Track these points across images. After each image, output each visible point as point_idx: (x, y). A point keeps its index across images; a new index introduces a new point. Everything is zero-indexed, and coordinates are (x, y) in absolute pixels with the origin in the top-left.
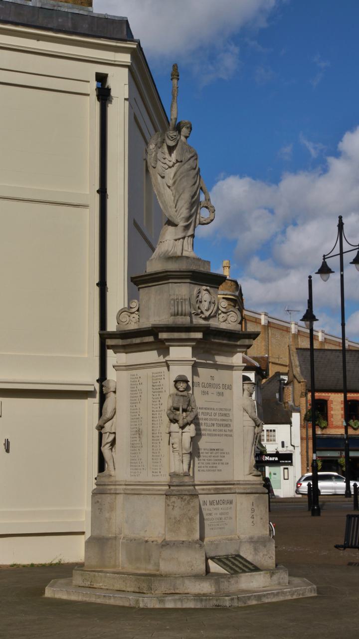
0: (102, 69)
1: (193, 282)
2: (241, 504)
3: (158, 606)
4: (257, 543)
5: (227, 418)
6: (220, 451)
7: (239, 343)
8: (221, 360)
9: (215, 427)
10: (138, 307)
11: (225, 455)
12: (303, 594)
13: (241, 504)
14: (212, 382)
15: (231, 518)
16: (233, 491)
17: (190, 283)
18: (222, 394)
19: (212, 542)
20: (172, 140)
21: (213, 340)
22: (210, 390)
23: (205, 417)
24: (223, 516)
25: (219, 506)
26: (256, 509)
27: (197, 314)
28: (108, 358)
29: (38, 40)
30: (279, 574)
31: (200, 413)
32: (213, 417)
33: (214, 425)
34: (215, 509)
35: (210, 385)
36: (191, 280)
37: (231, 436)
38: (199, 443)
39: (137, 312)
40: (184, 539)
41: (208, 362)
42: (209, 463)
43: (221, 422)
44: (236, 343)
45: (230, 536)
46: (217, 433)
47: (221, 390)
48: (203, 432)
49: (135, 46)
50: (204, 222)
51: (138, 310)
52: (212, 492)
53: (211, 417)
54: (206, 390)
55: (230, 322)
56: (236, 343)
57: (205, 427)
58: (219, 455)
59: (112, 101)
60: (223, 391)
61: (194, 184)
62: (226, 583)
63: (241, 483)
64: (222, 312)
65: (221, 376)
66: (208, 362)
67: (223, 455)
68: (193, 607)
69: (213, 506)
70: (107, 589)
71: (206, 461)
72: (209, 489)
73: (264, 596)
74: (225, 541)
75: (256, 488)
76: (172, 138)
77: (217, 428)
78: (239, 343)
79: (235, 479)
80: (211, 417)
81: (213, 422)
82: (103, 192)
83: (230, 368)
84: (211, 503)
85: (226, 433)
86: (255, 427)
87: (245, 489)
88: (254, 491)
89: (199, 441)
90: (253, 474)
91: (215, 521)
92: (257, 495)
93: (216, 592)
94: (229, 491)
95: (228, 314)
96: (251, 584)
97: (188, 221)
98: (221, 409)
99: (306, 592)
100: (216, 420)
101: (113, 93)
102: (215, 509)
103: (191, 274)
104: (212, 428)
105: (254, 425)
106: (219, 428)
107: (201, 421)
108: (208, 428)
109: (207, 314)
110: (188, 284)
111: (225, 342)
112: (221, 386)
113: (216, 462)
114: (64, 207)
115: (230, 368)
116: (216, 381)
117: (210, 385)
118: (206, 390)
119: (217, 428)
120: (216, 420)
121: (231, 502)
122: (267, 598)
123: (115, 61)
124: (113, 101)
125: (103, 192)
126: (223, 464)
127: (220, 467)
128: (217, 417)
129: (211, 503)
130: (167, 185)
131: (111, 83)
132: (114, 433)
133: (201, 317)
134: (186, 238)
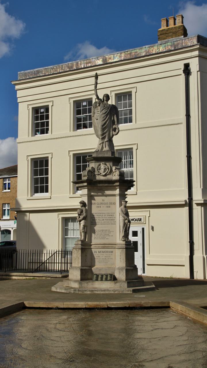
0: (186, 62)
2: (117, 253)
3: (56, 291)
4: (120, 269)
5: (113, 217)
7: (115, 185)
8: (107, 192)
12: (122, 292)
13: (117, 253)
14: (104, 202)
15: (112, 259)
16: (113, 247)
17: (95, 162)
18: (110, 207)
19: (97, 268)
21: (98, 185)
22: (102, 206)
23: (99, 217)
24: (107, 258)
26: (121, 255)
27: (98, 175)
28: (193, 189)
29: (159, 59)
30: (120, 283)
31: (96, 215)
33: (104, 220)
35: (102, 203)
36: (95, 161)
37: (115, 224)
38: (95, 228)
40: (76, 266)
41: (98, 194)
42: (98, 234)
44: (113, 185)
45: (111, 266)
47: (109, 205)
48: (97, 223)
49: (199, 47)
52: (100, 247)
56: (113, 185)
57: (99, 221)
59: (191, 74)
60: (111, 205)
61: (104, 120)
62: (86, 284)
63: (118, 244)
65: (107, 199)
66: (98, 194)
68: (64, 292)
72: (99, 247)
73: (96, 290)
74: (105, 268)
75: (122, 246)
78: (115, 185)
79: (117, 242)
82: (188, 116)
83: (114, 195)
84: (100, 252)
87: (119, 246)
88: (121, 247)
89: (95, 227)
92: (122, 249)
93: (79, 287)
94: (111, 247)
96: (102, 286)
97: (103, 136)
98: (109, 213)
99: (124, 291)
101: (191, 71)
103: (93, 158)
107: (96, 219)
109: (104, 174)
110: (94, 163)
111: (106, 185)
112: (109, 203)
114: (172, 126)
115: (114, 195)
116: (105, 202)
117: (102, 203)
121: (112, 252)
122: (98, 291)
123: (191, 56)
124: (192, 74)
125: (188, 116)
128: (106, 216)
129: (100, 252)
131: (191, 66)
133: (101, 175)
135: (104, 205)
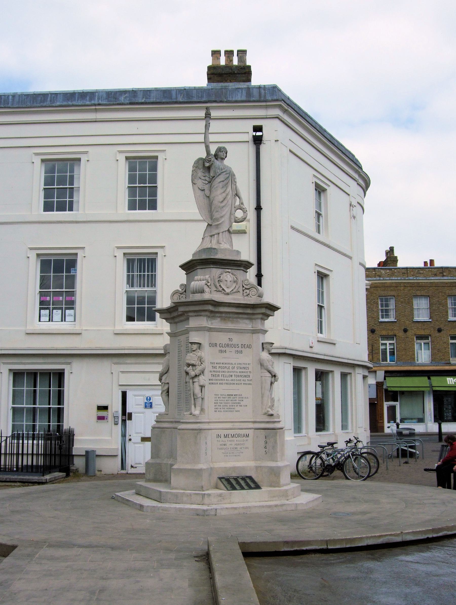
1: (154, 264)
6: (238, 396)
9: (233, 378)
10: (185, 288)
11: (244, 399)
14: (230, 343)
20: (208, 162)
22: (228, 349)
23: (223, 370)
25: (235, 439)
32: (231, 370)
34: (231, 441)
35: (228, 345)
39: (184, 293)
43: (240, 374)
46: (235, 382)
47: (240, 349)
50: (238, 220)
51: (185, 291)
53: (228, 370)
54: (224, 349)
55: (251, 296)
58: (238, 399)
60: (243, 349)
64: (245, 288)
67: (242, 399)
69: (228, 439)
70: (389, 491)
71: (223, 404)
76: (208, 160)
77: (235, 378)
80: (228, 370)
81: (231, 374)
85: (244, 382)
86: (272, 377)
90: (267, 414)
91: (230, 450)
95: (250, 289)
100: (233, 372)
102: (231, 441)
104: (230, 378)
105: (271, 376)
106: (238, 378)
108: (225, 378)
113: (234, 404)
116: (235, 342)
117: (228, 345)
118: (224, 349)
119: (235, 378)
120: (233, 372)
126: (240, 406)
127: (237, 408)
130: (206, 196)
132: (168, 383)
134: (221, 234)
135: (231, 349)
